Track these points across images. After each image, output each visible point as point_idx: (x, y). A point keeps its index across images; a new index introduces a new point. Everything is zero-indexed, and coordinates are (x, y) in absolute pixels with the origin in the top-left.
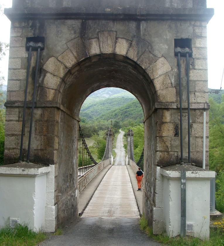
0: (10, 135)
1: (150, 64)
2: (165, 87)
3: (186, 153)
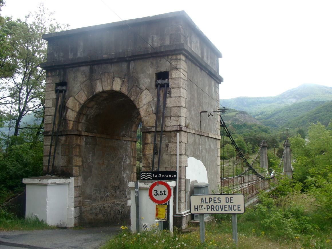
0: (46, 156)
1: (137, 96)
2: (147, 114)
3: (163, 168)
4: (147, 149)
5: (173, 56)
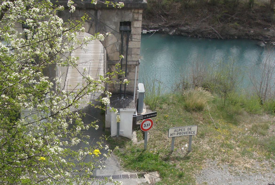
2: (113, 52)
5: (135, 10)
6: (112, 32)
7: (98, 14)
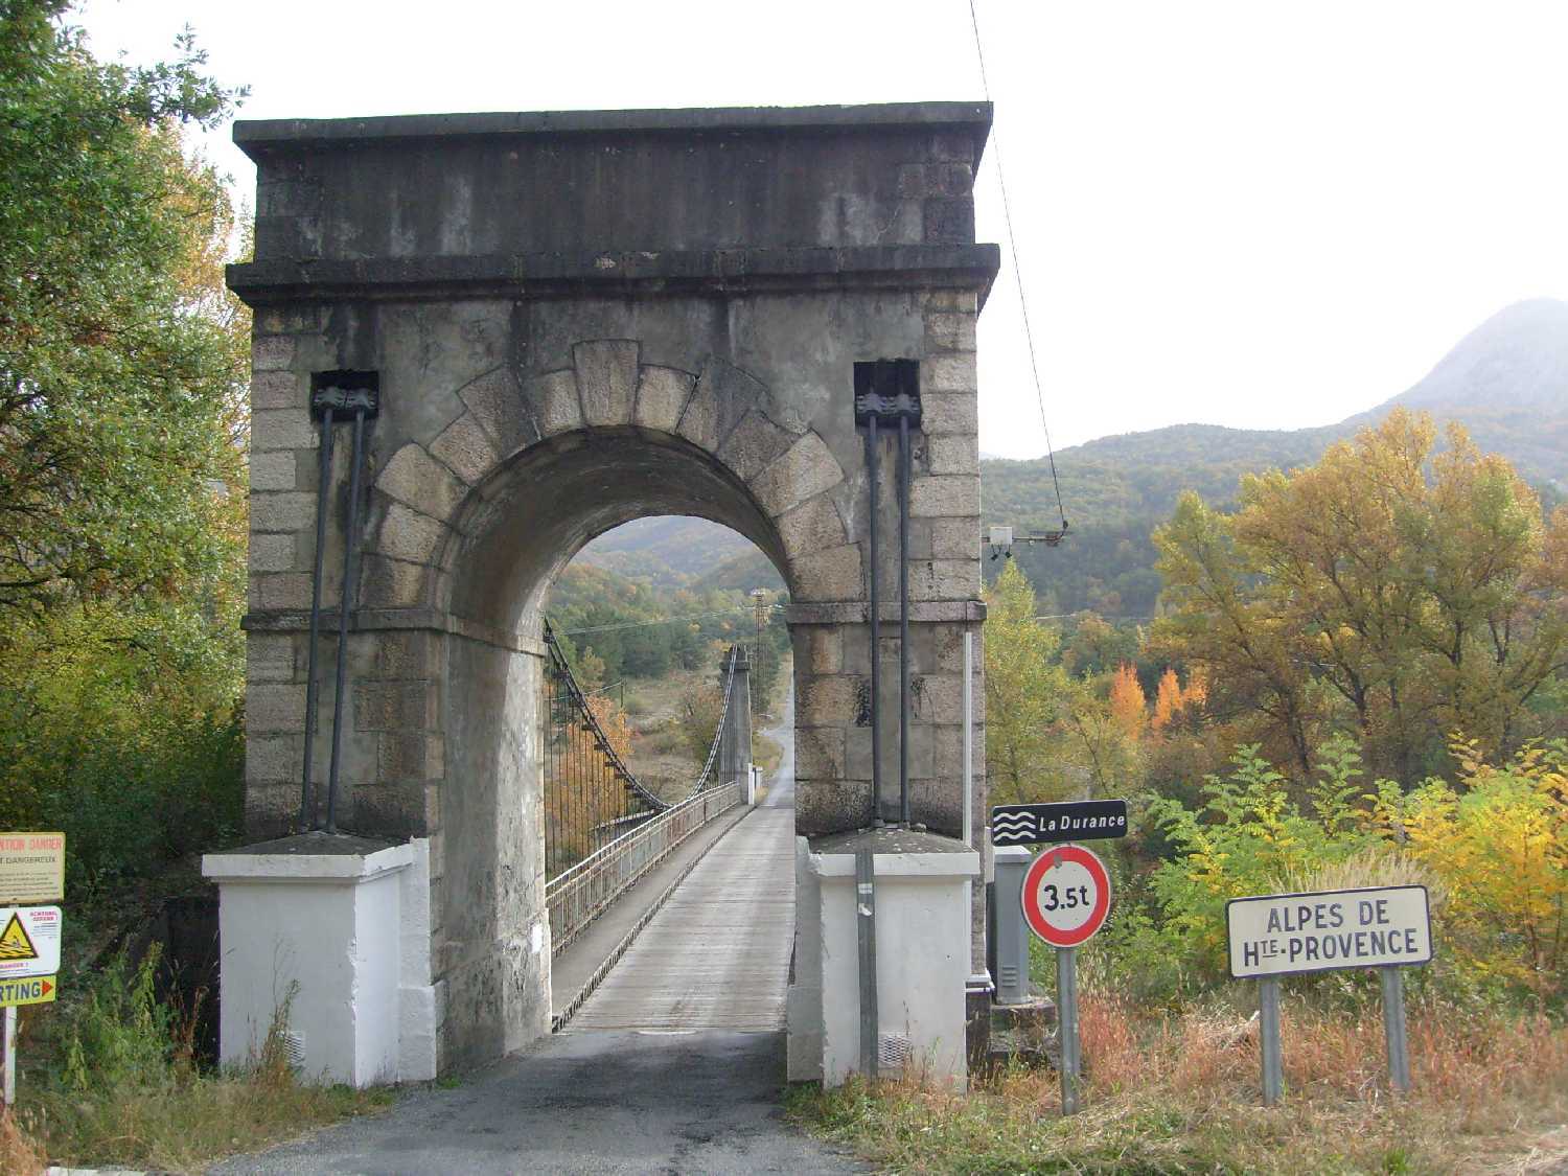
1: (765, 460)
2: (820, 545)
4: (818, 703)
6: (810, 423)
7: (731, 322)
